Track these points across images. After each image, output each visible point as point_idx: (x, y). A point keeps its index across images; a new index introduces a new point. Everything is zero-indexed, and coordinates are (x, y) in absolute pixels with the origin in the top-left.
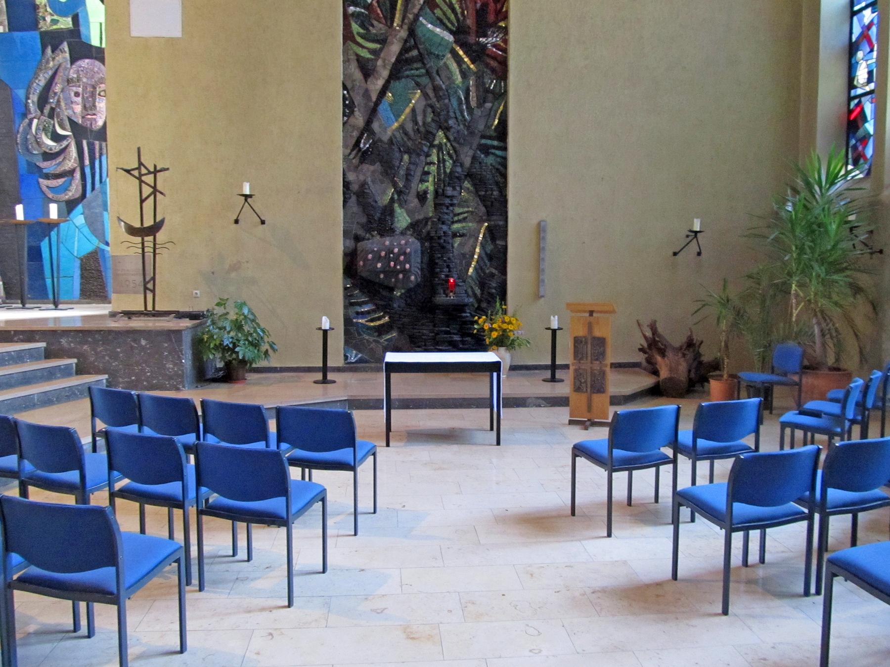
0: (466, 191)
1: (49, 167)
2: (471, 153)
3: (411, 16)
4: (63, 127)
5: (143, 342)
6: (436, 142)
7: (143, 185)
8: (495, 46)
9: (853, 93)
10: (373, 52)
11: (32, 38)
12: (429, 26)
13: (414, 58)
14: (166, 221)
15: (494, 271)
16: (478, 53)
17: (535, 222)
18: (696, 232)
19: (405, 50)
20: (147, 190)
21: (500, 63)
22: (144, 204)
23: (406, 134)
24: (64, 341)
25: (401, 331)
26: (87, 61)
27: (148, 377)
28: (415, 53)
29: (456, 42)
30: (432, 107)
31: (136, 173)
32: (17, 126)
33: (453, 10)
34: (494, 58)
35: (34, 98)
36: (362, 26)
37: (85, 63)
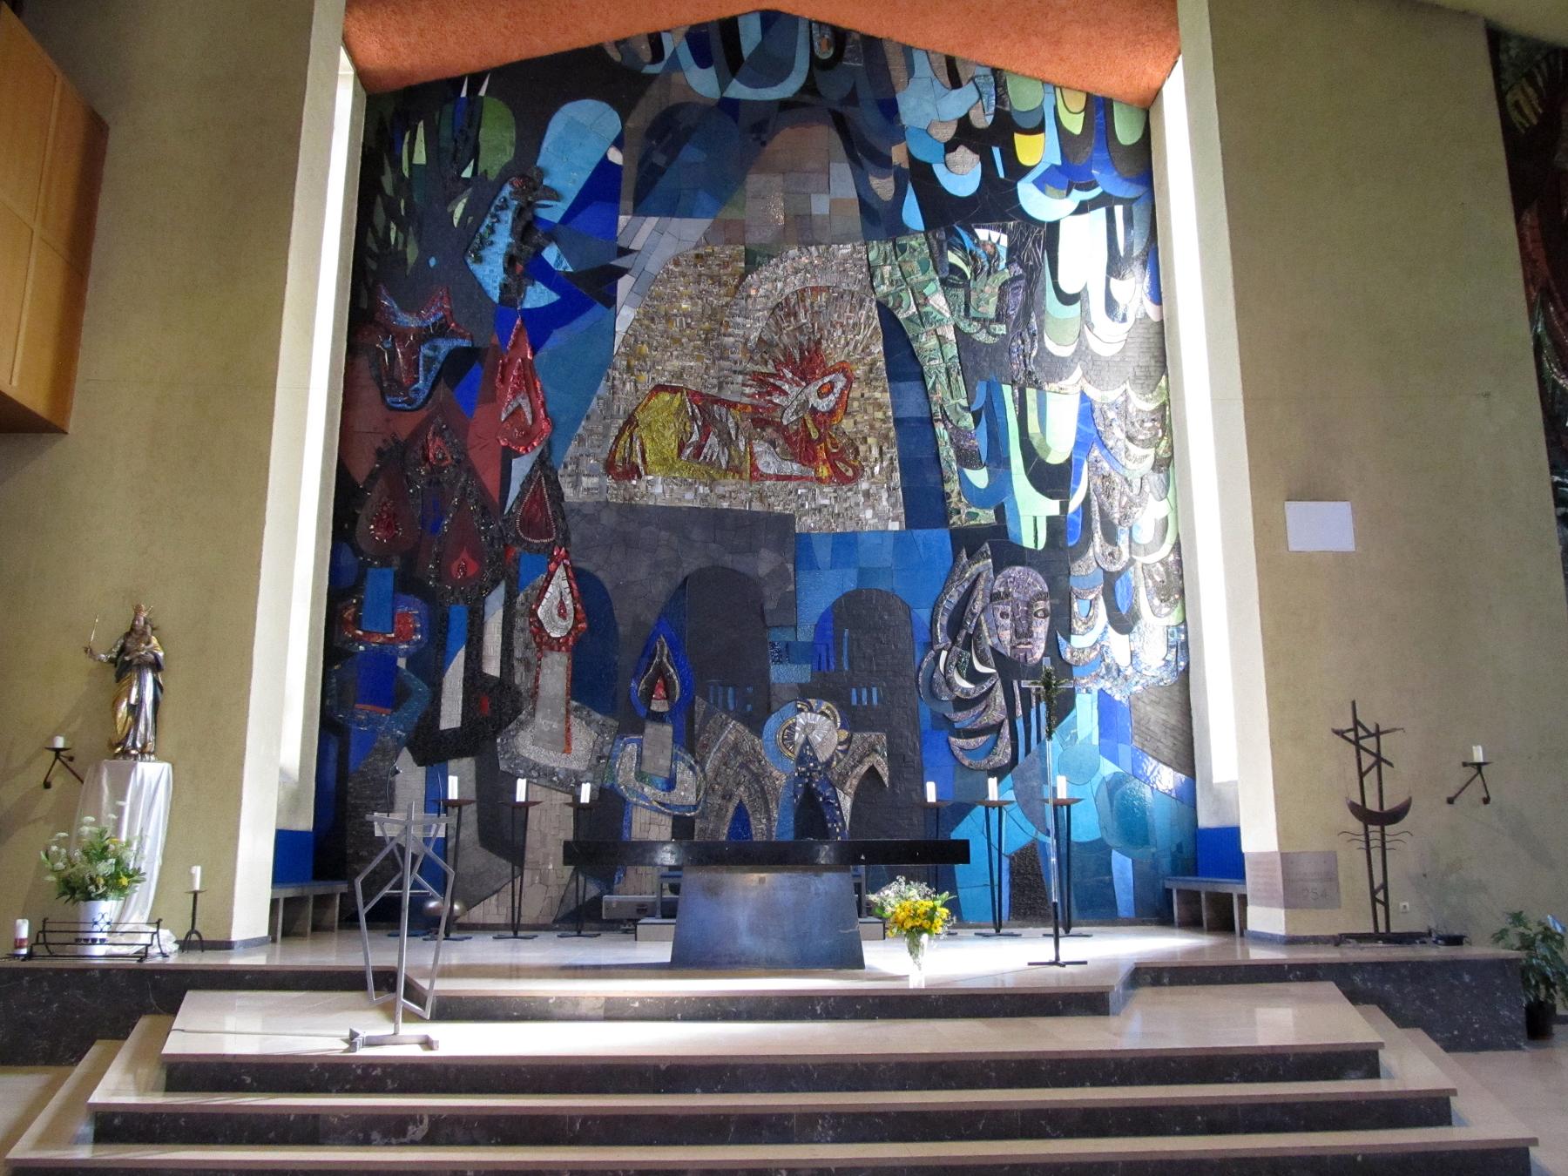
1: (963, 719)
4: (983, 662)
5: (1467, 978)
11: (939, 538)
20: (1367, 760)
22: (1365, 780)
24: (1357, 979)
26: (1018, 568)
32: (918, 659)
35: (943, 620)
37: (1016, 571)
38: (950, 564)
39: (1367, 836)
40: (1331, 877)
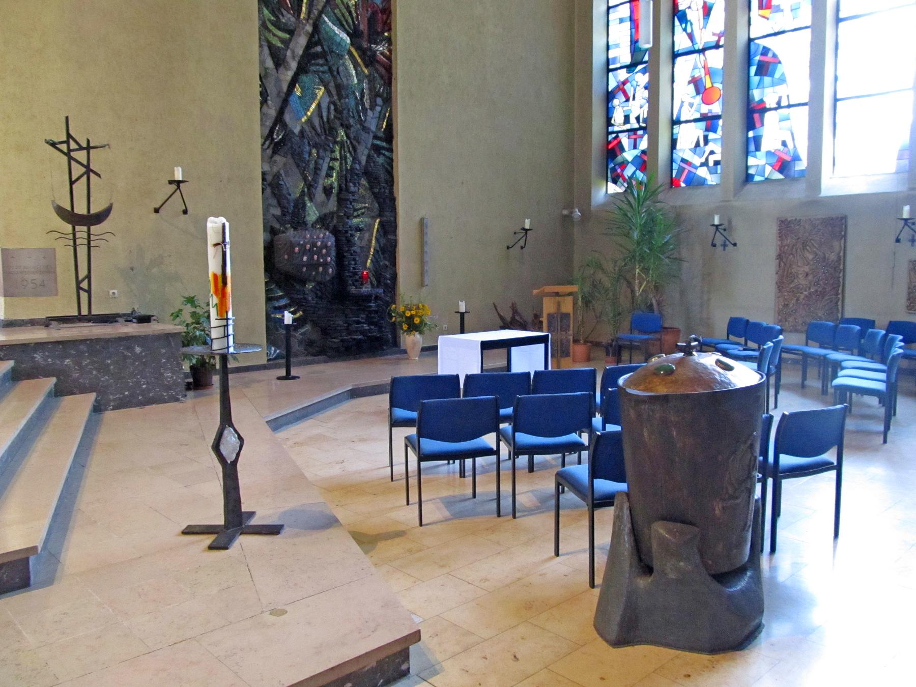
0: (362, 188)
2: (366, 152)
3: (316, 12)
5: (138, 350)
6: (339, 139)
7: (85, 163)
8: (382, 53)
9: (610, 129)
10: (283, 41)
12: (330, 24)
13: (317, 54)
14: (114, 206)
15: (387, 263)
16: (370, 59)
17: (418, 219)
18: (526, 230)
19: (309, 46)
20: (78, 170)
21: (385, 68)
22: (74, 186)
23: (314, 128)
24: (38, 357)
25: (315, 324)
27: (144, 390)
28: (319, 49)
29: (352, 44)
30: (335, 104)
31: (64, 147)
33: (350, 13)
34: (383, 65)
36: (273, 12)
38: (499, 310)
39: (74, 234)
40: (50, 270)
